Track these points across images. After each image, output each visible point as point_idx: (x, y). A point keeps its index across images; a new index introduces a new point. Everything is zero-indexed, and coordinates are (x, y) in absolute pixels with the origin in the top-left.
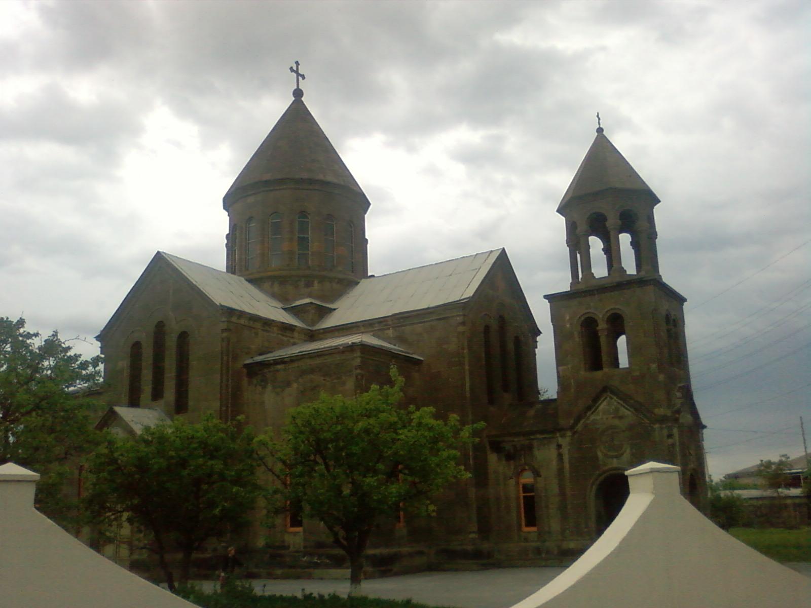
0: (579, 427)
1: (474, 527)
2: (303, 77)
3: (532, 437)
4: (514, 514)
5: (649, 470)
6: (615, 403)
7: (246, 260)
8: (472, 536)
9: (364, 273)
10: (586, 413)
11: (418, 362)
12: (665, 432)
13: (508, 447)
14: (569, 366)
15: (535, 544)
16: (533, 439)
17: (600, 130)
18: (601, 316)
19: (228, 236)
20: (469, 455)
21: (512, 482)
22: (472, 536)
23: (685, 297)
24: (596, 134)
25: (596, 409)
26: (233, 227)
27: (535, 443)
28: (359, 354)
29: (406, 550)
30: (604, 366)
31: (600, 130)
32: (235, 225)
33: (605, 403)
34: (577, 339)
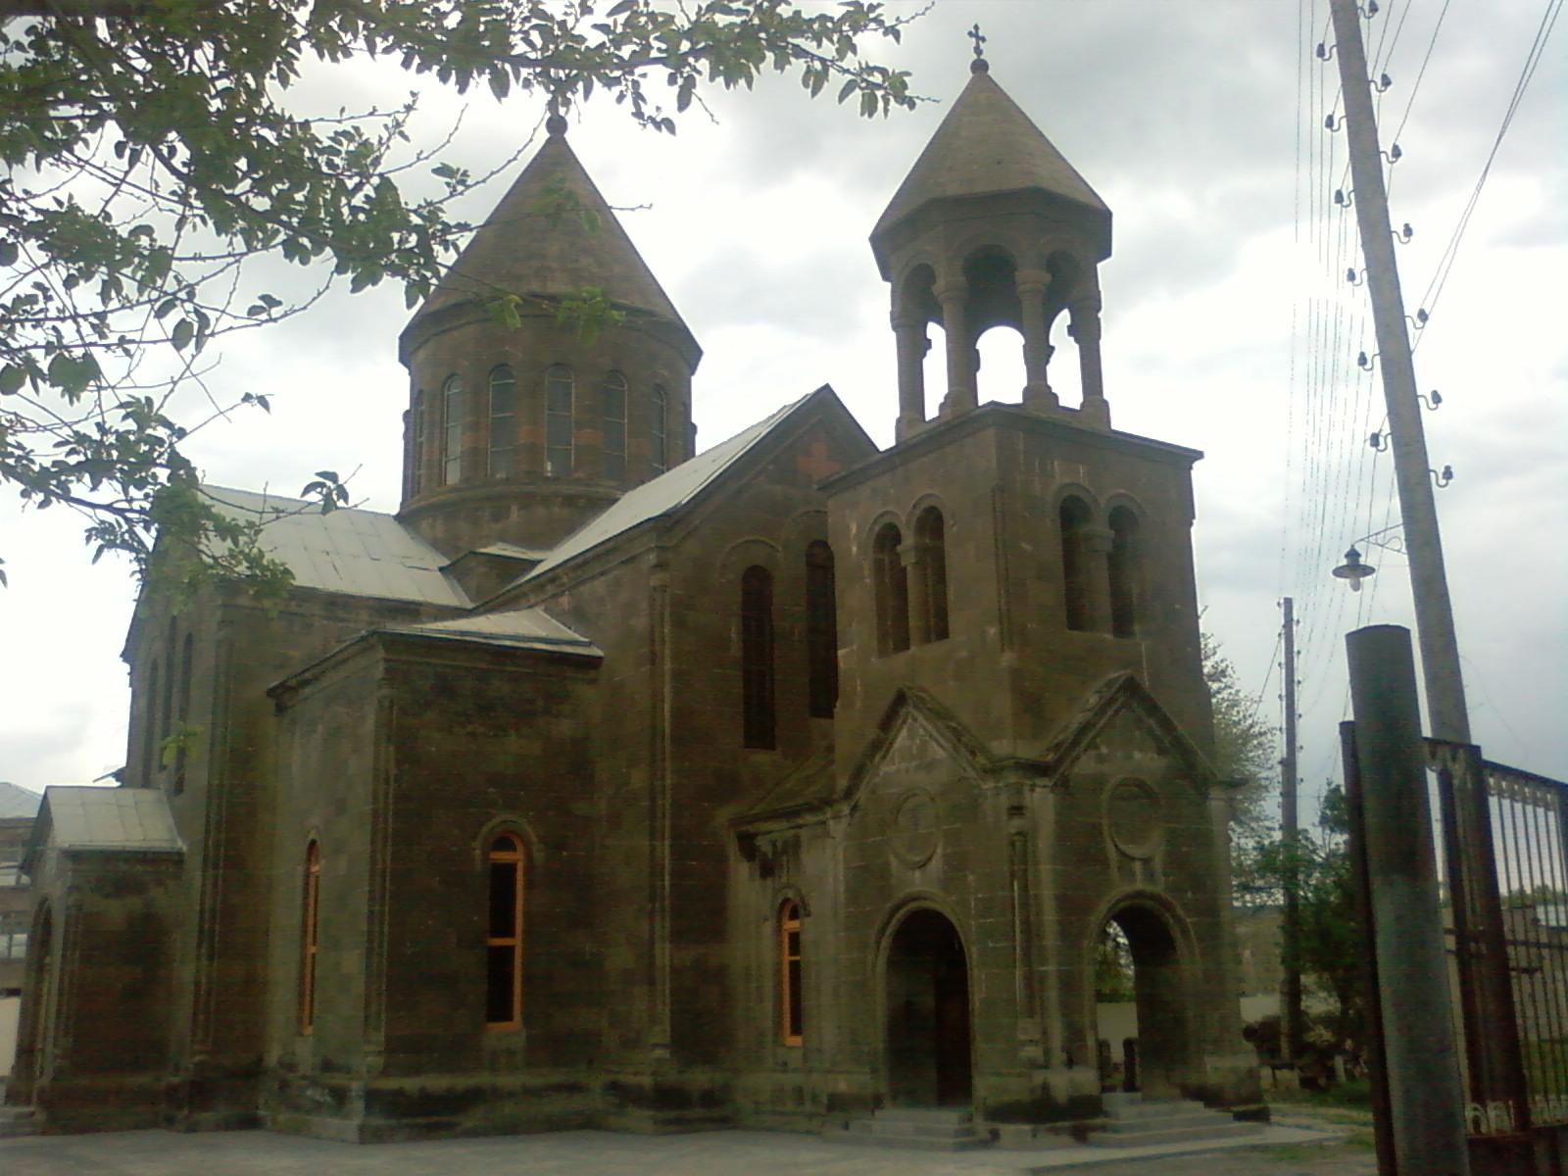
0: (862, 795)
1: (661, 1033)
2: (970, 34)
3: (800, 821)
4: (769, 1006)
5: (33, 974)
6: (921, 731)
7: (440, 465)
8: (659, 1053)
9: (693, 455)
10: (873, 756)
11: (593, 663)
12: (1004, 801)
13: (763, 844)
14: (855, 647)
15: (797, 1079)
16: (800, 827)
17: (980, 67)
18: (903, 518)
19: (406, 415)
20: (663, 865)
21: (768, 928)
22: (659, 1053)
23: (1199, 449)
24: (971, 75)
25: (888, 751)
26: (417, 396)
27: (804, 833)
28: (381, 653)
29: (506, 1081)
30: (911, 642)
31: (980, 67)
32: (421, 392)
33: (904, 732)
34: (868, 581)
